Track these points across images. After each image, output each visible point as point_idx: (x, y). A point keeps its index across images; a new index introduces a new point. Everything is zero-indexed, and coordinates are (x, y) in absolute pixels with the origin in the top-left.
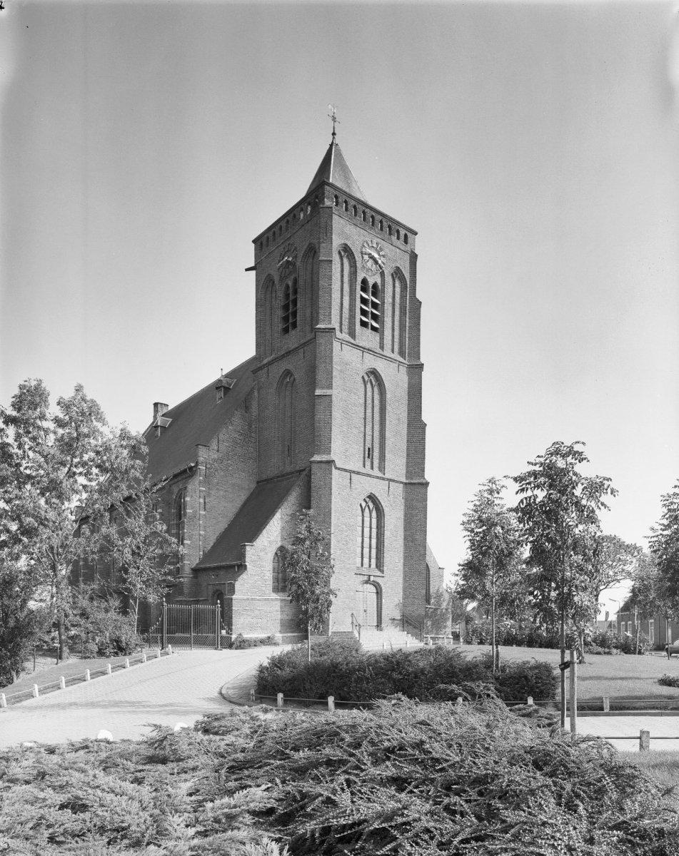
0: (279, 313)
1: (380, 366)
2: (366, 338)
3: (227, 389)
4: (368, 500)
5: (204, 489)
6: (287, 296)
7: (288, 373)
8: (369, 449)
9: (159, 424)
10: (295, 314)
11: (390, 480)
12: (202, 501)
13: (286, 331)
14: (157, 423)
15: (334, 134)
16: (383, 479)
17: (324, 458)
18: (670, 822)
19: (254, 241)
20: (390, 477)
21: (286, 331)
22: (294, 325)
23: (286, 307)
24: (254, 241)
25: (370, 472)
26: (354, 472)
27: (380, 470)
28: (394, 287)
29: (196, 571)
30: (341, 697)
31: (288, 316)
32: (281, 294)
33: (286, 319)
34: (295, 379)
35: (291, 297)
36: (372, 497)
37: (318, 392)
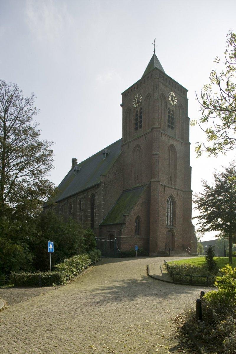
0: (133, 122)
1: (175, 143)
2: (170, 132)
3: (107, 154)
4: (170, 198)
5: (104, 193)
6: (137, 115)
7: (138, 146)
8: (170, 177)
9: (76, 169)
10: (141, 122)
11: (178, 190)
12: (103, 198)
13: (136, 129)
14: (75, 169)
15: (154, 51)
16: (176, 189)
17: (156, 179)
18: (1, 300)
19: (122, 94)
20: (178, 188)
21: (136, 129)
22: (141, 127)
23: (137, 120)
24: (122, 94)
25: (171, 186)
26: (166, 186)
27: (174, 186)
28: (180, 112)
29: (101, 226)
30: (174, 279)
31: (137, 123)
32: (134, 114)
33: (136, 124)
34: (141, 148)
35: (139, 115)
36: (171, 197)
37: (154, 153)
